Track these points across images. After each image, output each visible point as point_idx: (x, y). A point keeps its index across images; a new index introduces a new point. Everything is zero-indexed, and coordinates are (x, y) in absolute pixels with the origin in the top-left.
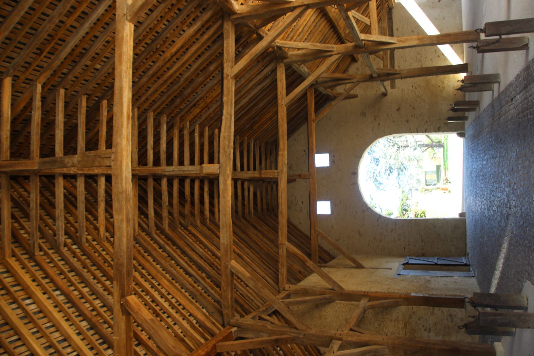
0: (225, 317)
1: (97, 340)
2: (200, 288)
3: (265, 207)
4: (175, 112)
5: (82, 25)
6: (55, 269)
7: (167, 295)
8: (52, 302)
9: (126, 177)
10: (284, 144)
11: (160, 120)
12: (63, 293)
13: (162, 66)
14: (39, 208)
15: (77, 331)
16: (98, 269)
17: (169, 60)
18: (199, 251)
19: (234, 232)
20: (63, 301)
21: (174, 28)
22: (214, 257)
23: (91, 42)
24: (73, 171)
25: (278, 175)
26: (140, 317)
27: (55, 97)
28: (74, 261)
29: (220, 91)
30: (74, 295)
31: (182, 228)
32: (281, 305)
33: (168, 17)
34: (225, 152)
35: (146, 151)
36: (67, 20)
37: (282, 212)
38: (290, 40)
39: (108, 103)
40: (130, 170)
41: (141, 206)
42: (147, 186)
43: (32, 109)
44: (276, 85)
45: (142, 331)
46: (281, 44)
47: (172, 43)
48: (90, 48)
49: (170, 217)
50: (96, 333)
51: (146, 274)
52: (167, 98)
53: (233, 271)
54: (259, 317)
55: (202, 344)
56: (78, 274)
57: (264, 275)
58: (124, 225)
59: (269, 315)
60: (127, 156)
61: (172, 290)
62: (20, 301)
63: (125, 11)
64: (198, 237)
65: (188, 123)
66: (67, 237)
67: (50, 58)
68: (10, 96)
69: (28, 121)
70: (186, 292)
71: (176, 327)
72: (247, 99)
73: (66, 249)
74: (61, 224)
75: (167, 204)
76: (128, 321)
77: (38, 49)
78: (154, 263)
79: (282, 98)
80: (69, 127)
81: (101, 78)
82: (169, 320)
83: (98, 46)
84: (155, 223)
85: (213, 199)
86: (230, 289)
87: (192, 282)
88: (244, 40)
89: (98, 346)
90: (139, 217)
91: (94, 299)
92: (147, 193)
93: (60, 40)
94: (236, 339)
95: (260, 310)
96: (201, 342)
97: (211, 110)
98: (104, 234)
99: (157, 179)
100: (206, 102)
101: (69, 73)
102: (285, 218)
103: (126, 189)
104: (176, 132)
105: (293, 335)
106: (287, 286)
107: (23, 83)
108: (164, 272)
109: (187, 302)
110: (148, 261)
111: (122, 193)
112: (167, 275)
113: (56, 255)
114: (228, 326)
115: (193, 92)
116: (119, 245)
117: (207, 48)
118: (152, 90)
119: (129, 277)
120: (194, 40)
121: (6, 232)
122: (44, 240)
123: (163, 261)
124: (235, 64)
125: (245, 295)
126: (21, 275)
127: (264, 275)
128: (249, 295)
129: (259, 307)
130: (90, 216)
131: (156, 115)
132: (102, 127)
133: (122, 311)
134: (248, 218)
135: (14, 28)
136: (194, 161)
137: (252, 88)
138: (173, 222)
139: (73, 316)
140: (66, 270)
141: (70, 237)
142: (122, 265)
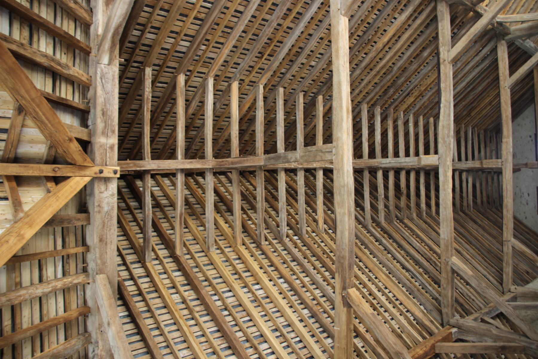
0: (445, 316)
1: (317, 329)
2: (417, 284)
3: (485, 199)
4: (389, 102)
5: (297, 25)
6: (279, 258)
7: (384, 289)
8: (277, 289)
9: (348, 171)
10: (508, 130)
11: (374, 112)
12: (286, 281)
13: (375, 57)
14: (264, 200)
15: (300, 318)
16: (317, 260)
17: (381, 50)
18: (416, 245)
19: (455, 229)
20: (287, 289)
21: (385, 17)
22: (431, 252)
23: (305, 41)
24: (293, 166)
25: (502, 165)
26: (361, 310)
27: (275, 96)
28: (295, 251)
29: (437, 75)
30: (297, 284)
31: (398, 221)
32: (508, 308)
33: (379, 7)
34: (445, 142)
35: (361, 143)
36: (284, 23)
37: (507, 206)
38: (512, 14)
39: (323, 98)
40: (351, 164)
41: (357, 198)
42: (363, 180)
43: (256, 109)
44: (497, 65)
45: (360, 323)
46: (502, 19)
47: (384, 33)
48: (306, 46)
49: (386, 210)
50: (316, 322)
51: (363, 267)
52: (380, 90)
53: (454, 268)
54: (481, 319)
55: (420, 342)
56: (300, 264)
57: (485, 273)
58: (346, 218)
59: (492, 318)
60: (348, 150)
61: (390, 284)
62: (251, 286)
63: (339, 6)
64: (414, 231)
65: (402, 113)
66: (288, 228)
67: (270, 60)
68: (238, 99)
69: (252, 120)
70: (403, 287)
71: (393, 322)
72: (464, 84)
73: (288, 239)
74: (283, 215)
75: (383, 196)
76: (349, 313)
77: (259, 53)
78: (371, 256)
79: (505, 80)
80: (288, 123)
81: (317, 75)
82: (386, 314)
83: (313, 44)
84: (371, 216)
85: (430, 191)
86: (450, 287)
87: (410, 277)
88: (459, 20)
89: (319, 334)
90: (356, 210)
91: (314, 289)
92: (363, 187)
93: (278, 42)
94: (456, 341)
95: (483, 312)
96: (418, 340)
97: (426, 98)
98: (322, 226)
99: (373, 171)
100: (420, 91)
101: (287, 72)
102: (511, 212)
103: (347, 182)
104: (390, 123)
105: (523, 344)
106: (513, 288)
107: (248, 85)
108: (381, 266)
109: (404, 297)
110: (365, 254)
111: (344, 186)
112: (384, 269)
113: (280, 245)
114: (448, 326)
115: (406, 81)
116: (342, 238)
117: (420, 34)
118: (365, 82)
119: (350, 270)
120: (406, 27)
121: (237, 223)
122: (269, 231)
123: (379, 255)
124: (452, 47)
125: (465, 294)
126: (250, 262)
127: (485, 273)
128: (470, 294)
129: (481, 309)
130: (308, 209)
131: (370, 107)
132: (319, 122)
133: (343, 303)
134: (467, 211)
135: (240, 36)
136: (398, 152)
137: (469, 72)
138: (389, 215)
139: (296, 303)
140: (289, 260)
141: (291, 228)
142: (344, 258)
